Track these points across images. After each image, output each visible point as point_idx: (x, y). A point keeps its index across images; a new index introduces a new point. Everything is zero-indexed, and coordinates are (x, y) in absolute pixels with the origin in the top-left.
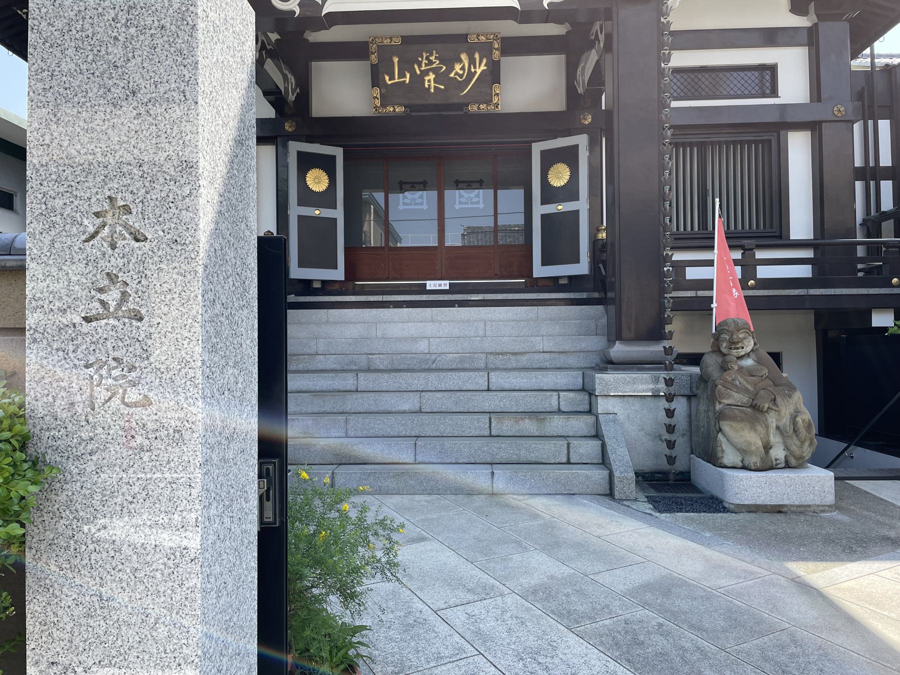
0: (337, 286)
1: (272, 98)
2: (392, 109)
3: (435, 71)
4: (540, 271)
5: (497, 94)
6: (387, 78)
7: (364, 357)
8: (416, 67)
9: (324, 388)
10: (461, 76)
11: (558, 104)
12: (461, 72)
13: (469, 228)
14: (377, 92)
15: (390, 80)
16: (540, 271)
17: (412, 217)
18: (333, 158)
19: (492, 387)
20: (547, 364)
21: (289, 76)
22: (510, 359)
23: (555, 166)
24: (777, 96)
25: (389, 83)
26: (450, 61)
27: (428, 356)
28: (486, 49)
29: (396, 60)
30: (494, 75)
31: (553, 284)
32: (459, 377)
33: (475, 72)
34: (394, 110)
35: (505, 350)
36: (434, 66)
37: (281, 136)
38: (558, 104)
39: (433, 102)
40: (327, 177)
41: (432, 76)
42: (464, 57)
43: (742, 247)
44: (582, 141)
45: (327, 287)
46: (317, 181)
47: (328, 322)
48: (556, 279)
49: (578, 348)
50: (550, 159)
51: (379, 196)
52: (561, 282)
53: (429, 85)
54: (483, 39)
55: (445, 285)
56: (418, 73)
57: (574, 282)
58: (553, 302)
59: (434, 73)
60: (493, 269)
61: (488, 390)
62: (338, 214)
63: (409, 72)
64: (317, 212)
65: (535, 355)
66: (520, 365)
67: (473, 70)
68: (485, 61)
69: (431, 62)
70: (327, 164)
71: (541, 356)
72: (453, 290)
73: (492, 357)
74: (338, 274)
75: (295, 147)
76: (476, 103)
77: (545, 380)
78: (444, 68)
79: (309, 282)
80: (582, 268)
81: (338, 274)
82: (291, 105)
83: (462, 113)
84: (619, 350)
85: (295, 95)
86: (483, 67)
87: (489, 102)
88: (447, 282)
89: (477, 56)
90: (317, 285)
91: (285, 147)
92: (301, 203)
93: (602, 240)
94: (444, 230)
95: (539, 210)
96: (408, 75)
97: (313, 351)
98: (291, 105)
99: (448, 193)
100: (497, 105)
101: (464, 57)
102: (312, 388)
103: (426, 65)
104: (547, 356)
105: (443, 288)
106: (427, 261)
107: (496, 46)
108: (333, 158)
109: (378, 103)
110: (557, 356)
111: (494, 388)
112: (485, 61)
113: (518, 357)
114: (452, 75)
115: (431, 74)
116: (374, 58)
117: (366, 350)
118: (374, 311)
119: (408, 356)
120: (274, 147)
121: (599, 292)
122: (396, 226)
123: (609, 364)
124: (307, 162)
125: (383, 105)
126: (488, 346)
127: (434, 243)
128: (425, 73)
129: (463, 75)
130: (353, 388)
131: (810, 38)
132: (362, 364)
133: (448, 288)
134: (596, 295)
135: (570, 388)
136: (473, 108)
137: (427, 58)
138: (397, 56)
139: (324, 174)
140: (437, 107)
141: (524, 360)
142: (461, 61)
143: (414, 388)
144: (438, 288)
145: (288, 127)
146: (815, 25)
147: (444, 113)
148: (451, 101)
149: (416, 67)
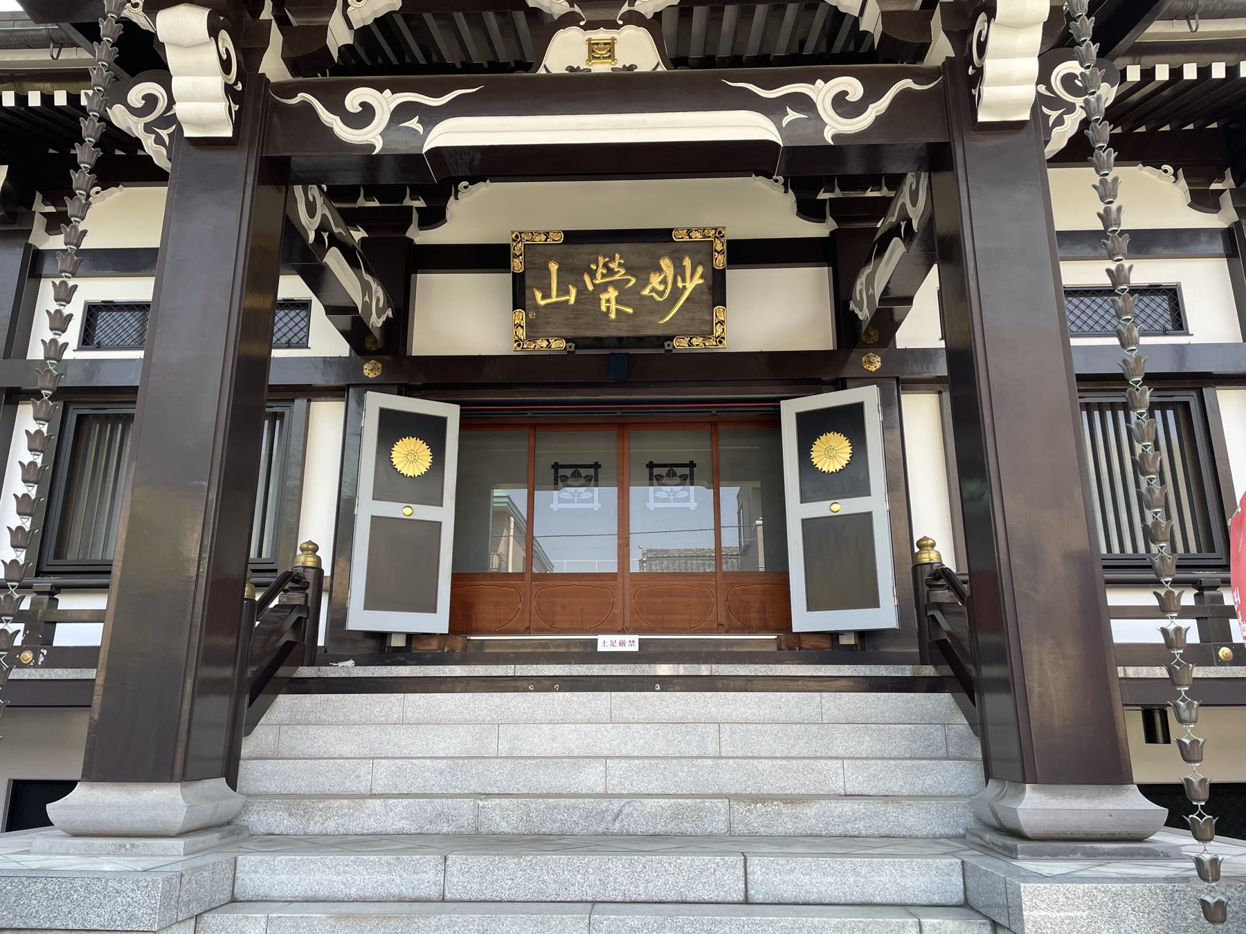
0: (434, 645)
1: (346, 320)
2: (545, 344)
3: (615, 284)
4: (804, 620)
5: (722, 323)
6: (538, 295)
7: (467, 804)
8: (587, 278)
9: (368, 893)
10: (661, 294)
11: (821, 338)
12: (661, 288)
13: (650, 551)
14: (520, 316)
15: (543, 298)
16: (804, 620)
17: (574, 527)
18: (441, 422)
19: (756, 895)
20: (861, 827)
21: (374, 285)
22: (779, 814)
23: (823, 438)
24: (1187, 334)
25: (542, 303)
26: (642, 271)
27: (605, 804)
28: (702, 251)
29: (554, 267)
30: (716, 291)
31: (829, 647)
32: (679, 867)
33: (684, 287)
34: (549, 346)
35: (766, 789)
36: (617, 277)
37: (354, 385)
38: (821, 338)
39: (614, 333)
40: (428, 452)
41: (612, 294)
42: (666, 264)
43: (1194, 583)
44: (868, 396)
45: (415, 648)
46: (411, 457)
47: (403, 722)
48: (834, 636)
49: (918, 789)
50: (812, 426)
51: (519, 496)
52: (844, 641)
53: (608, 308)
54: (697, 236)
55: (629, 643)
56: (590, 288)
57: (867, 644)
58: (843, 683)
59: (616, 288)
60: (731, 622)
61: (746, 902)
62: (445, 514)
63: (575, 286)
64: (408, 511)
65: (833, 804)
66: (802, 827)
67: (680, 285)
68: (700, 270)
69: (611, 272)
70: (431, 431)
71: (847, 807)
72: (646, 655)
73: (740, 808)
74: (437, 622)
75: (376, 401)
76: (687, 335)
77: (876, 879)
78: (633, 281)
79: (383, 637)
80: (884, 615)
81: (437, 622)
82: (377, 334)
83: (662, 351)
84: (1036, 806)
85: (384, 318)
86: (697, 281)
87: (708, 334)
88: (636, 638)
89: (687, 262)
90: (398, 642)
91: (361, 402)
92: (379, 495)
93: (931, 564)
94: (628, 545)
95: (797, 511)
96: (573, 291)
97: (363, 788)
98: (377, 334)
99: (635, 492)
100: (720, 340)
101: (666, 264)
102: (340, 891)
103: (603, 276)
104: (859, 807)
105: (627, 648)
106: (594, 600)
107: (719, 247)
108: (441, 422)
109: (522, 333)
110: (879, 807)
111: (759, 898)
112: (700, 270)
113: (798, 808)
114: (646, 292)
115: (611, 289)
116: (517, 265)
117: (474, 787)
118: (496, 698)
119: (563, 802)
120: (343, 404)
121: (934, 663)
122: (544, 543)
123: (1008, 836)
124: (394, 427)
125: (531, 338)
126: (732, 778)
127: (609, 565)
128: (604, 288)
129: (664, 291)
130: (434, 892)
131: (1232, 244)
132: (463, 821)
133: (636, 648)
134: (929, 671)
135: (936, 899)
136: (681, 344)
137: (605, 265)
138: (556, 261)
139: (425, 446)
140: (620, 341)
141: (810, 817)
142: (659, 270)
143: (575, 893)
144: (618, 649)
145: (370, 370)
146: (1238, 224)
147: (632, 351)
148: (643, 333)
149: (587, 278)
